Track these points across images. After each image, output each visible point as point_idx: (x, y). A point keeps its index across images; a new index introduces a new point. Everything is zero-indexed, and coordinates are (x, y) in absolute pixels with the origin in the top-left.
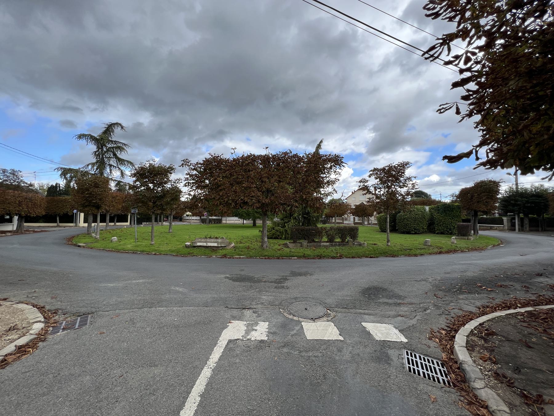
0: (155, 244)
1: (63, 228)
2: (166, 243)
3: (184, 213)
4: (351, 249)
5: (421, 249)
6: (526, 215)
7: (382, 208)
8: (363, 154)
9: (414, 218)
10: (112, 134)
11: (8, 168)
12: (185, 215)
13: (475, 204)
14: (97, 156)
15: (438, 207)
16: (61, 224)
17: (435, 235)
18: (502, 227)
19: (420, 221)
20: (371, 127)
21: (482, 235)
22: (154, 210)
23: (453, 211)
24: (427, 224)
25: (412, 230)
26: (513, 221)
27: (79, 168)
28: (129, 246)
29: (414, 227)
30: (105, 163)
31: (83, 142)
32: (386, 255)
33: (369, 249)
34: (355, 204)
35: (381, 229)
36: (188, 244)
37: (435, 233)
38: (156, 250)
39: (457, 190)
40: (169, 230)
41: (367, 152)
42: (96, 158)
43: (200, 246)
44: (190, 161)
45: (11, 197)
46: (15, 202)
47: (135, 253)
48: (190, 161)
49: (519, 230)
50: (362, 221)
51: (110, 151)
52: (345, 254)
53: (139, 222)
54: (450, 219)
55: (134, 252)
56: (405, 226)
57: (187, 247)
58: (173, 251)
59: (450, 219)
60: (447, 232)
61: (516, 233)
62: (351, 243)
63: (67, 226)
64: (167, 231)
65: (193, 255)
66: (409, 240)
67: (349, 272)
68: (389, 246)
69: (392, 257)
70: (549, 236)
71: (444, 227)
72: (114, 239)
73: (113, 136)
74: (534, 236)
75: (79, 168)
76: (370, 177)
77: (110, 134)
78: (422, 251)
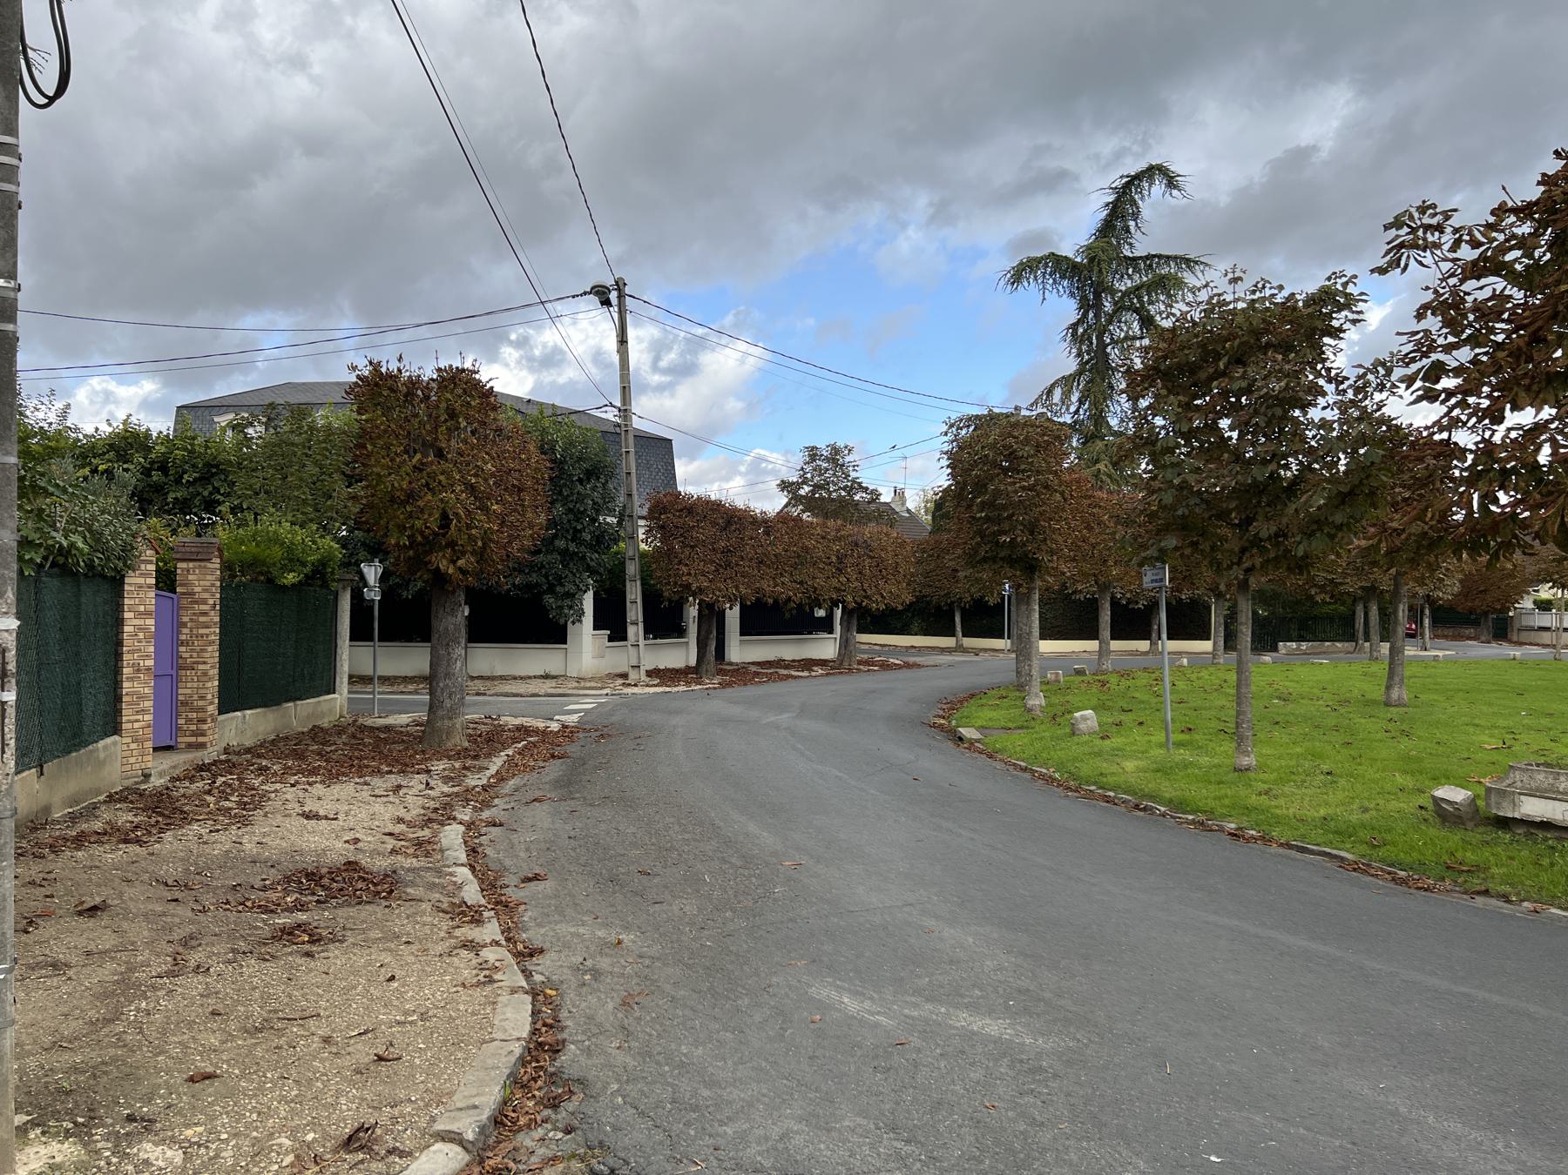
0: (1261, 768)
1: (972, 658)
2: (1325, 768)
3: (1521, 593)
10: (1132, 223)
11: (822, 444)
12: (1527, 603)
14: (1082, 342)
16: (970, 642)
22: (1248, 571)
27: (1016, 408)
28: (1130, 765)
30: (1112, 369)
31: (1030, 289)
36: (1455, 794)
38: (1248, 810)
40: (1389, 687)
42: (1079, 355)
43: (1546, 825)
44: (1447, 215)
45: (818, 542)
46: (829, 558)
47: (1145, 809)
48: (1447, 215)
51: (1129, 309)
53: (1266, 639)
55: (1140, 805)
57: (1446, 815)
58: (1345, 833)
63: (986, 650)
64: (1378, 693)
65: (1476, 883)
72: (1085, 718)
73: (1138, 235)
75: (1016, 408)
77: (1128, 231)
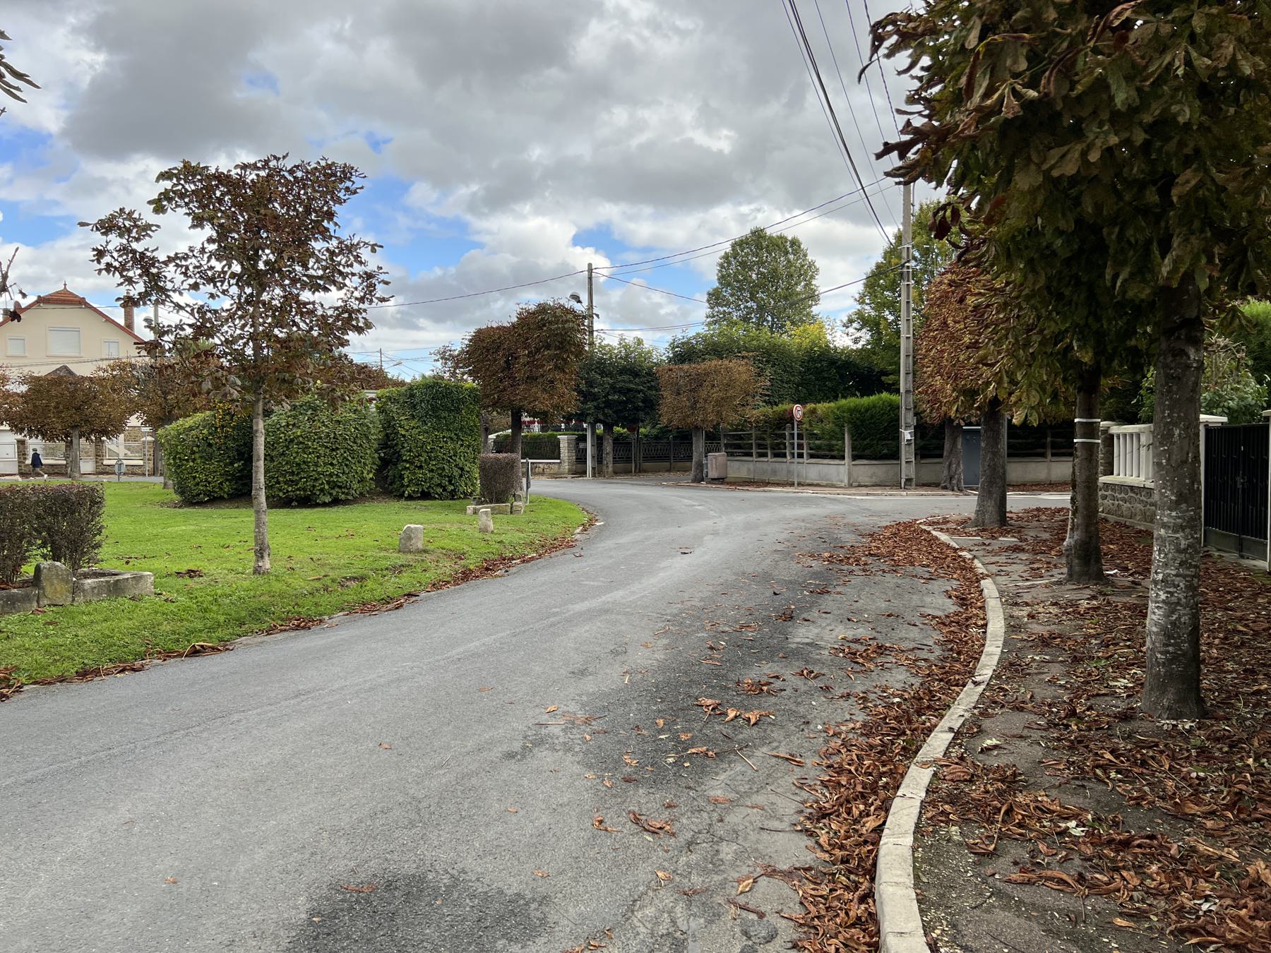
4: (64, 622)
5: (398, 569)
6: (608, 427)
7: (234, 385)
8: (50, 136)
9: (328, 436)
13: (522, 387)
15: (412, 396)
17: (403, 503)
18: (556, 466)
19: (351, 451)
20: (86, 17)
21: (539, 494)
23: (458, 410)
24: (374, 463)
25: (322, 490)
26: (581, 446)
29: (331, 475)
32: (265, 626)
33: (172, 607)
34: (26, 371)
35: (182, 493)
37: (400, 496)
39: (457, 338)
41: (65, 133)
49: (594, 475)
50: (66, 458)
52: (25, 661)
54: (451, 439)
56: (292, 473)
59: (451, 439)
60: (440, 490)
61: (588, 480)
62: (60, 587)
66: (327, 533)
67: (124, 811)
68: (266, 573)
69: (298, 628)
70: (656, 485)
71: (432, 471)
74: (644, 488)
76: (159, 206)
78: (405, 579)
